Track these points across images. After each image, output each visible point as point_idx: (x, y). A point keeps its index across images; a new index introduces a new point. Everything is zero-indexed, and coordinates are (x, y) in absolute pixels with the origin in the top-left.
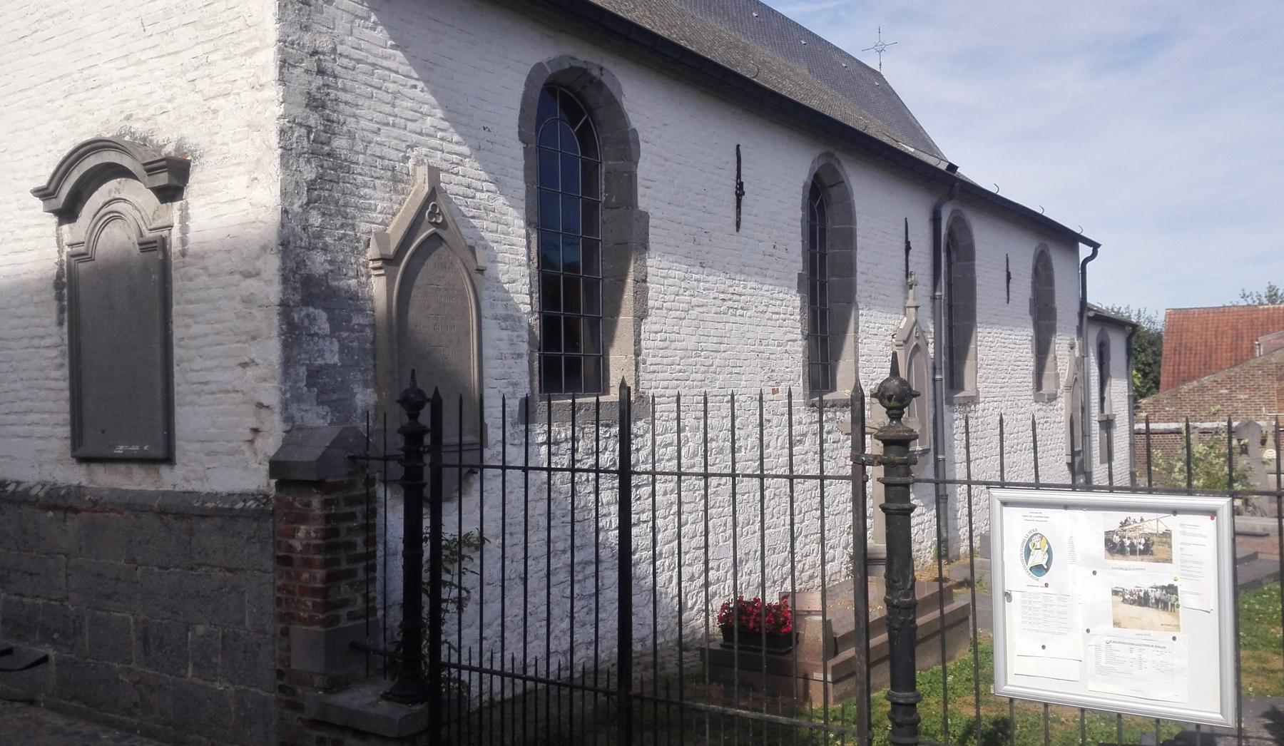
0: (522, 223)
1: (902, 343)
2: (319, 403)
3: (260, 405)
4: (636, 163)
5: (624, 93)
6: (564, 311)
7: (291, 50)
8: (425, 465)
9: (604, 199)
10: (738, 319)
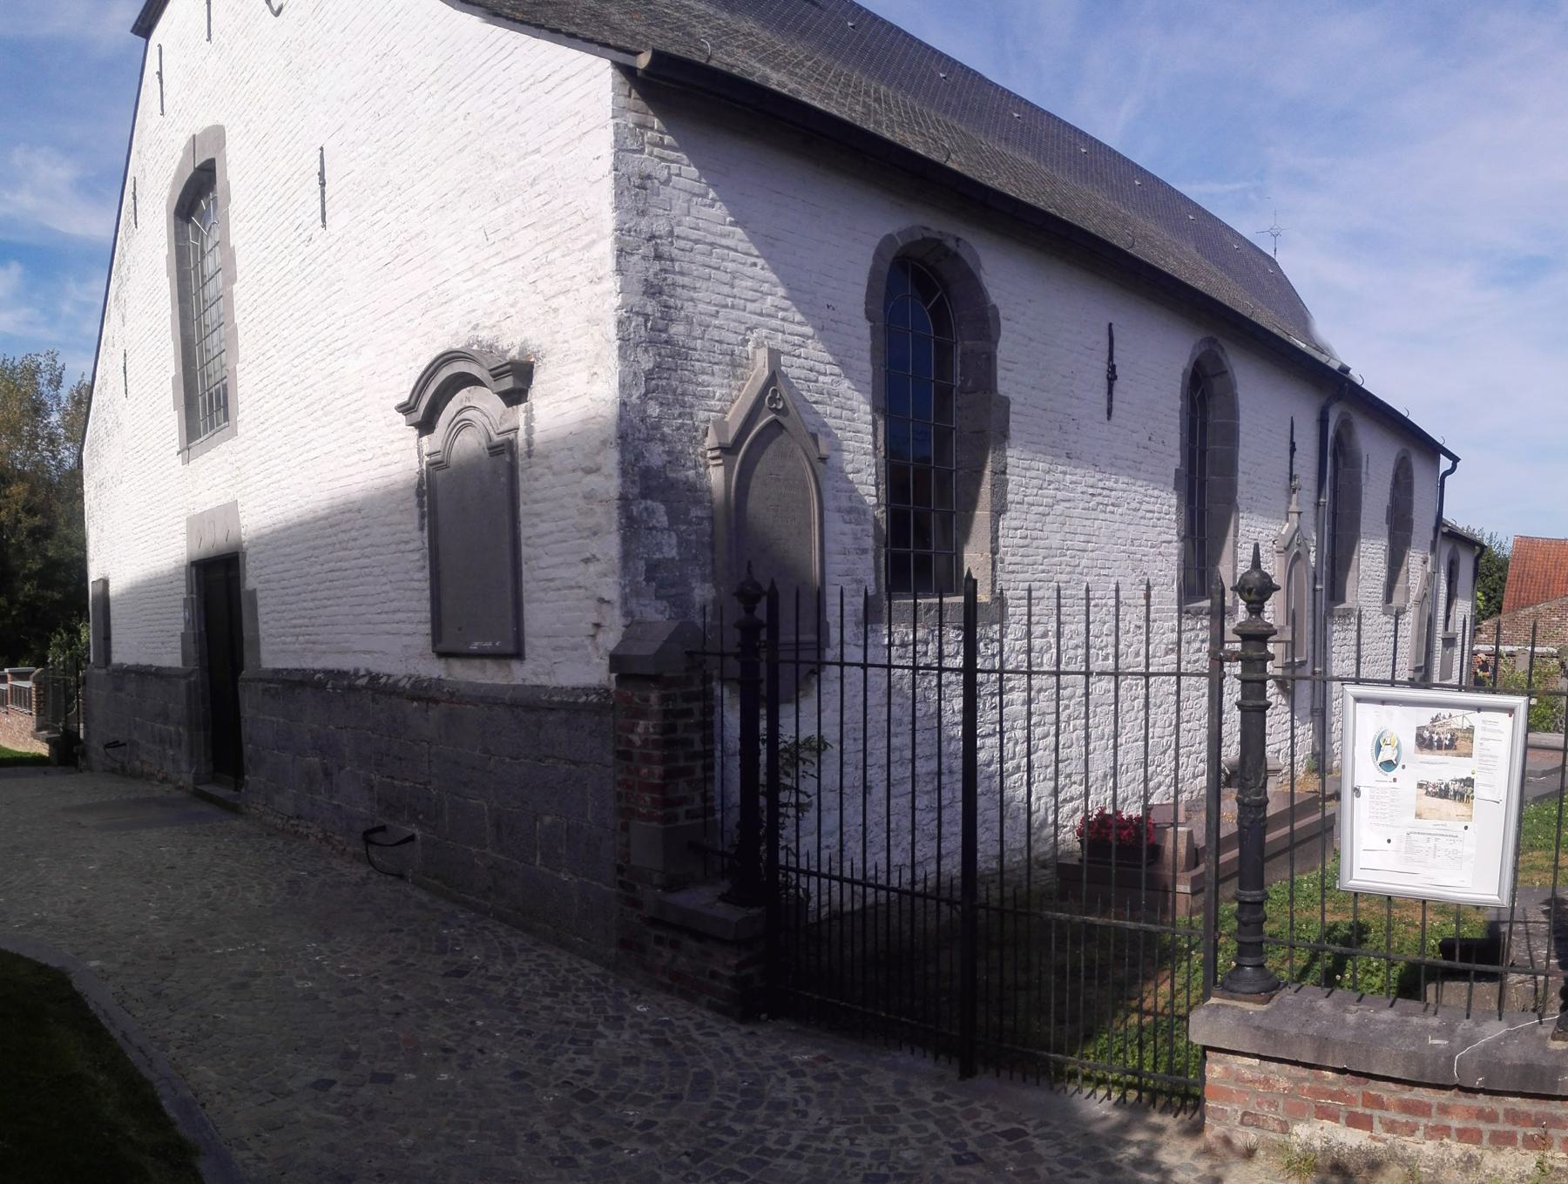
0: (868, 408)
1: (1282, 549)
2: (657, 598)
3: (602, 601)
4: (996, 343)
5: (983, 265)
6: (915, 547)
7: (627, 238)
8: (762, 661)
9: (959, 383)
10: (1108, 516)
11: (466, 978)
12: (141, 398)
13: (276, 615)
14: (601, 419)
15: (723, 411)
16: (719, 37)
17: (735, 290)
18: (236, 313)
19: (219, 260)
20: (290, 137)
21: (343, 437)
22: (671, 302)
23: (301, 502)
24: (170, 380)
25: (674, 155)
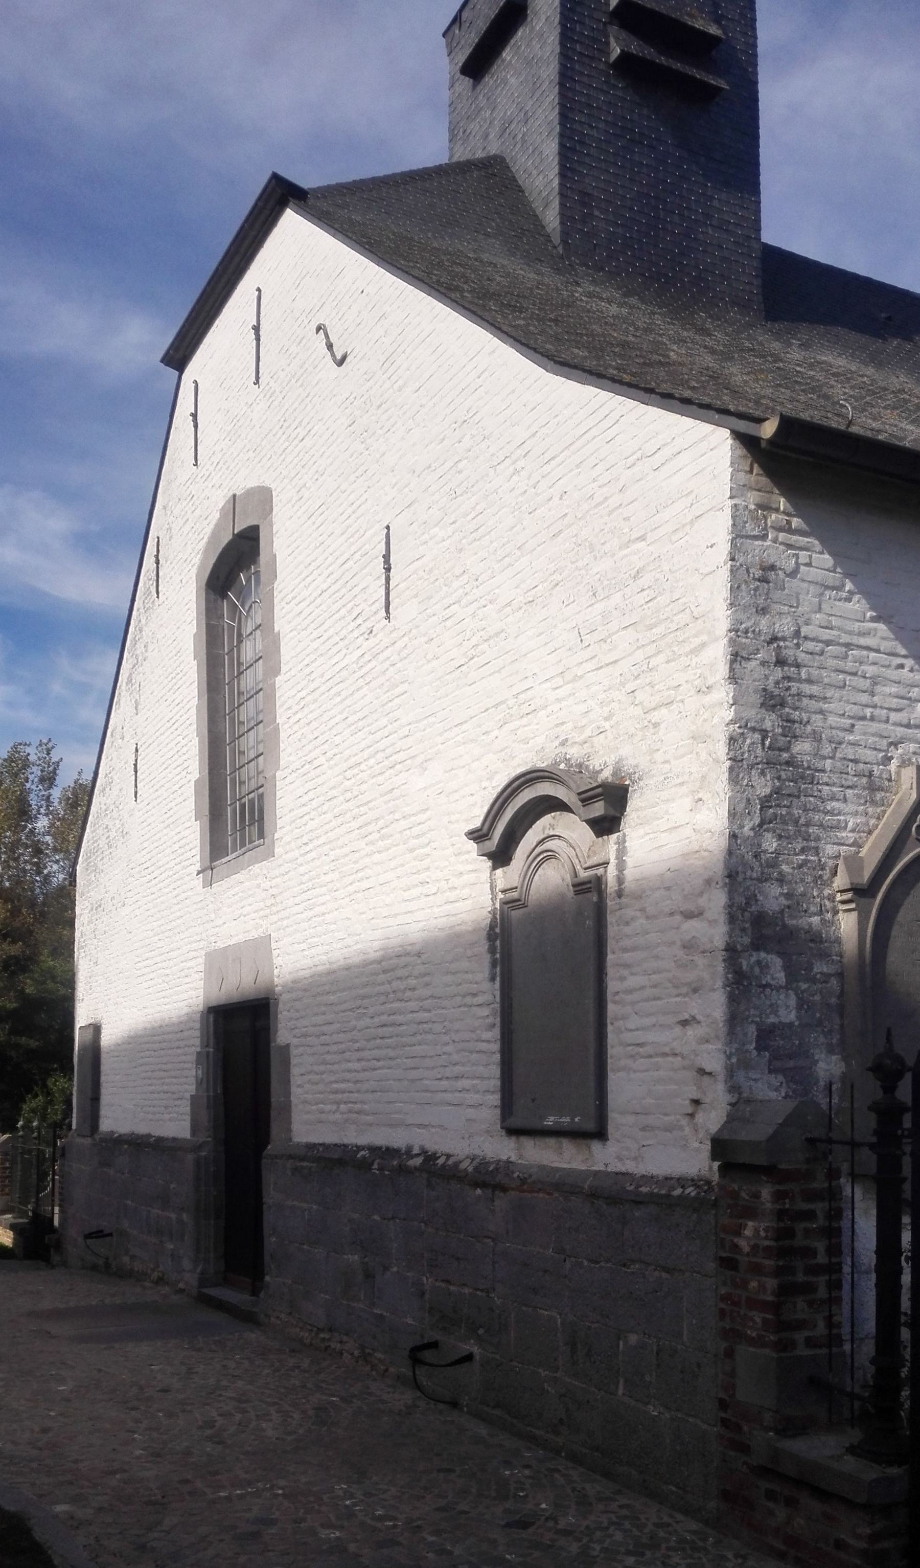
2: (770, 1072)
3: (702, 1072)
7: (744, 640)
8: (905, 1154)
11: (531, 1530)
12: (155, 802)
13: (316, 1078)
14: (706, 854)
15: (857, 845)
16: (863, 398)
17: (875, 698)
18: (279, 711)
19: (259, 646)
20: (350, 511)
21: (402, 865)
22: (796, 715)
23: (349, 941)
24: (192, 783)
25: (805, 540)
